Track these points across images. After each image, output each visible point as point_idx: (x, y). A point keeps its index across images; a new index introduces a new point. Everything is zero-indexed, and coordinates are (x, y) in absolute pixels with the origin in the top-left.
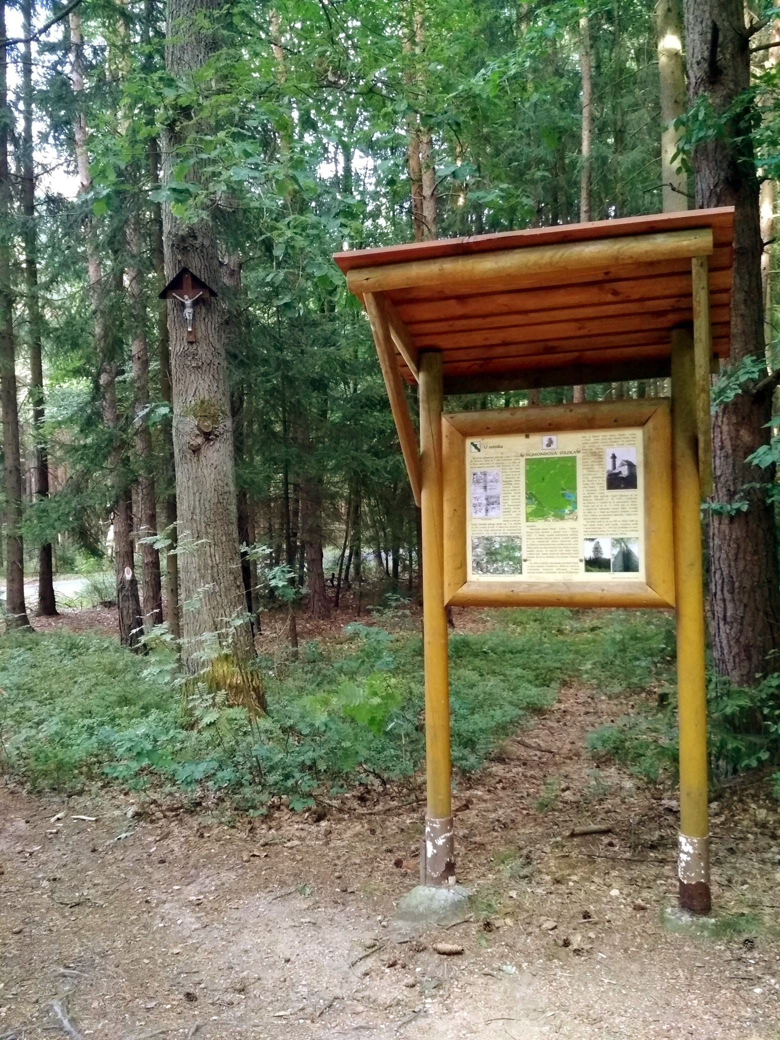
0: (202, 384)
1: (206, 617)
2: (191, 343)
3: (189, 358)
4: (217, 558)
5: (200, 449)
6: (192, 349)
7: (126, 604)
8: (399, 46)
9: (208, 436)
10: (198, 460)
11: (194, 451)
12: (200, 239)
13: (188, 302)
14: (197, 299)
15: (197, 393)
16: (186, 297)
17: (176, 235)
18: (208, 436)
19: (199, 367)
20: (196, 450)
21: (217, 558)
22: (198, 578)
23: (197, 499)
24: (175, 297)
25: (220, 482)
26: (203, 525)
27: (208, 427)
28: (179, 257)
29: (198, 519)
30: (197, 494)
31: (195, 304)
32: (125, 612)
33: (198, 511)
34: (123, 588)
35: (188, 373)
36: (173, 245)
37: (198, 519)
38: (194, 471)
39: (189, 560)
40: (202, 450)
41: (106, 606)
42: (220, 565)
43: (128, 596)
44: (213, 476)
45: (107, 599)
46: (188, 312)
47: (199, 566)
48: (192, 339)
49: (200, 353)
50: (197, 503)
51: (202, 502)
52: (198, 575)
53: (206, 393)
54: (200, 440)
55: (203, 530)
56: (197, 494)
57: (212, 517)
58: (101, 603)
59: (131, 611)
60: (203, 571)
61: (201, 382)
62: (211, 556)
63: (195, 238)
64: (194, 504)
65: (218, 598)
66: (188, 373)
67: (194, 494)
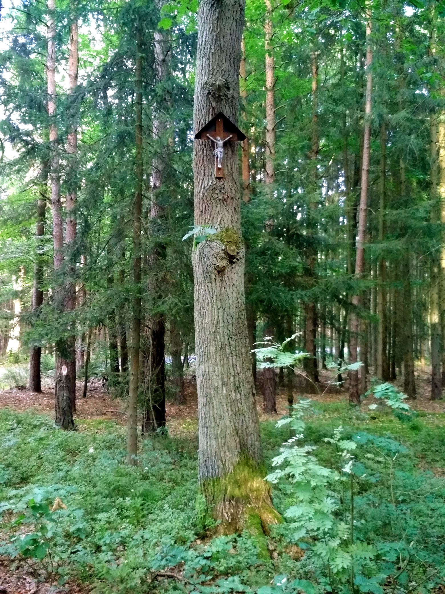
0: (227, 215)
1: (228, 422)
2: (219, 178)
3: (217, 192)
4: (238, 368)
5: (224, 270)
6: (220, 183)
7: (62, 393)
8: (298, 17)
9: (231, 259)
10: (222, 280)
11: (219, 272)
12: (231, 91)
13: (221, 143)
14: (228, 141)
15: (222, 222)
16: (219, 138)
17: (213, 85)
18: (231, 259)
19: (225, 200)
20: (221, 271)
21: (238, 368)
22: (220, 385)
23: (221, 314)
24: (208, 138)
25: (239, 300)
26: (226, 337)
27: (234, 251)
28: (214, 104)
29: (221, 331)
30: (221, 310)
31: (225, 145)
32: (60, 399)
33: (221, 325)
34: (60, 381)
35: (215, 205)
36: (209, 93)
37: (221, 331)
38: (218, 289)
39: (211, 368)
40: (226, 272)
41: (19, 389)
42: (241, 375)
43: (63, 387)
44: (235, 294)
45: (21, 384)
46: (219, 151)
47: (222, 374)
48: (220, 175)
49: (226, 187)
50: (221, 318)
51: (225, 316)
52: (220, 383)
53: (230, 222)
54: (225, 263)
55: (226, 342)
56: (221, 310)
57: (234, 331)
58: (16, 387)
59: (65, 398)
60: (225, 380)
61: (226, 213)
62: (233, 366)
63: (228, 89)
64: (218, 319)
65: (239, 405)
66: (215, 205)
67: (218, 309)
